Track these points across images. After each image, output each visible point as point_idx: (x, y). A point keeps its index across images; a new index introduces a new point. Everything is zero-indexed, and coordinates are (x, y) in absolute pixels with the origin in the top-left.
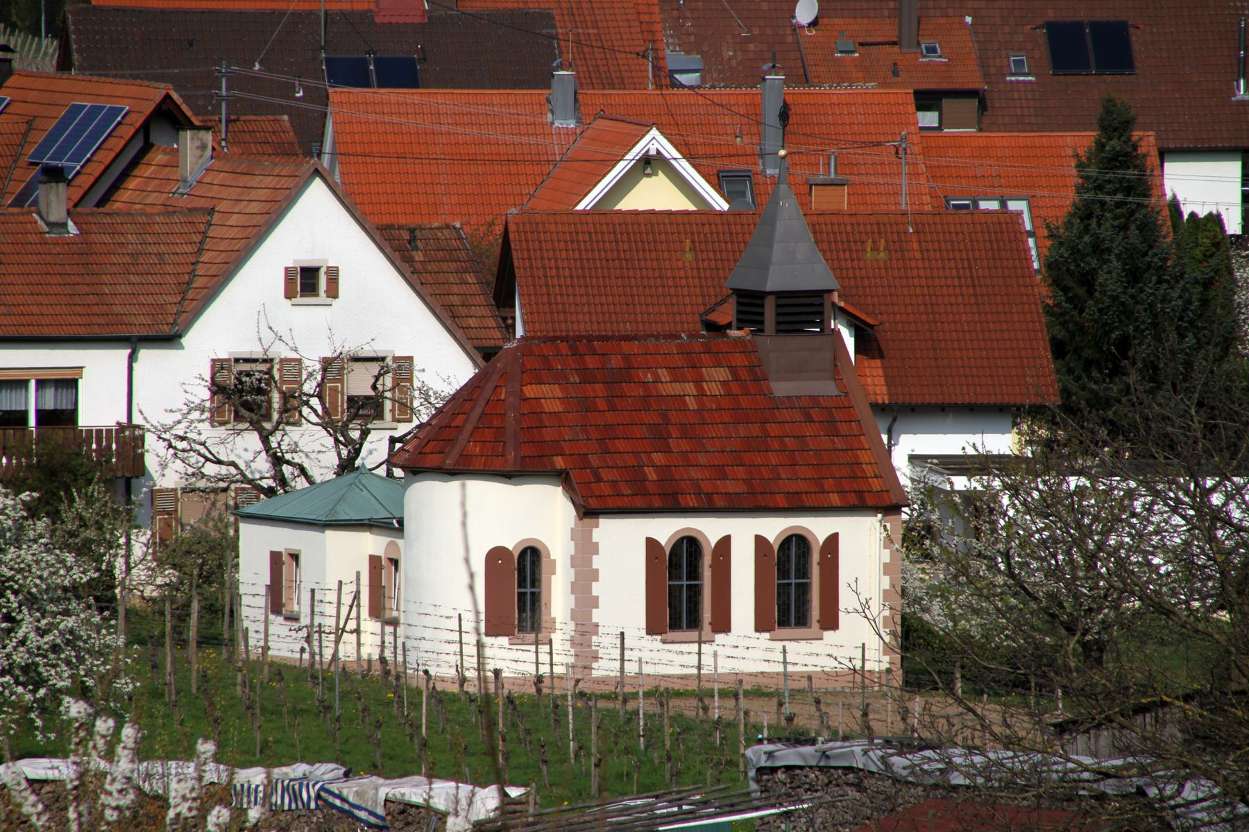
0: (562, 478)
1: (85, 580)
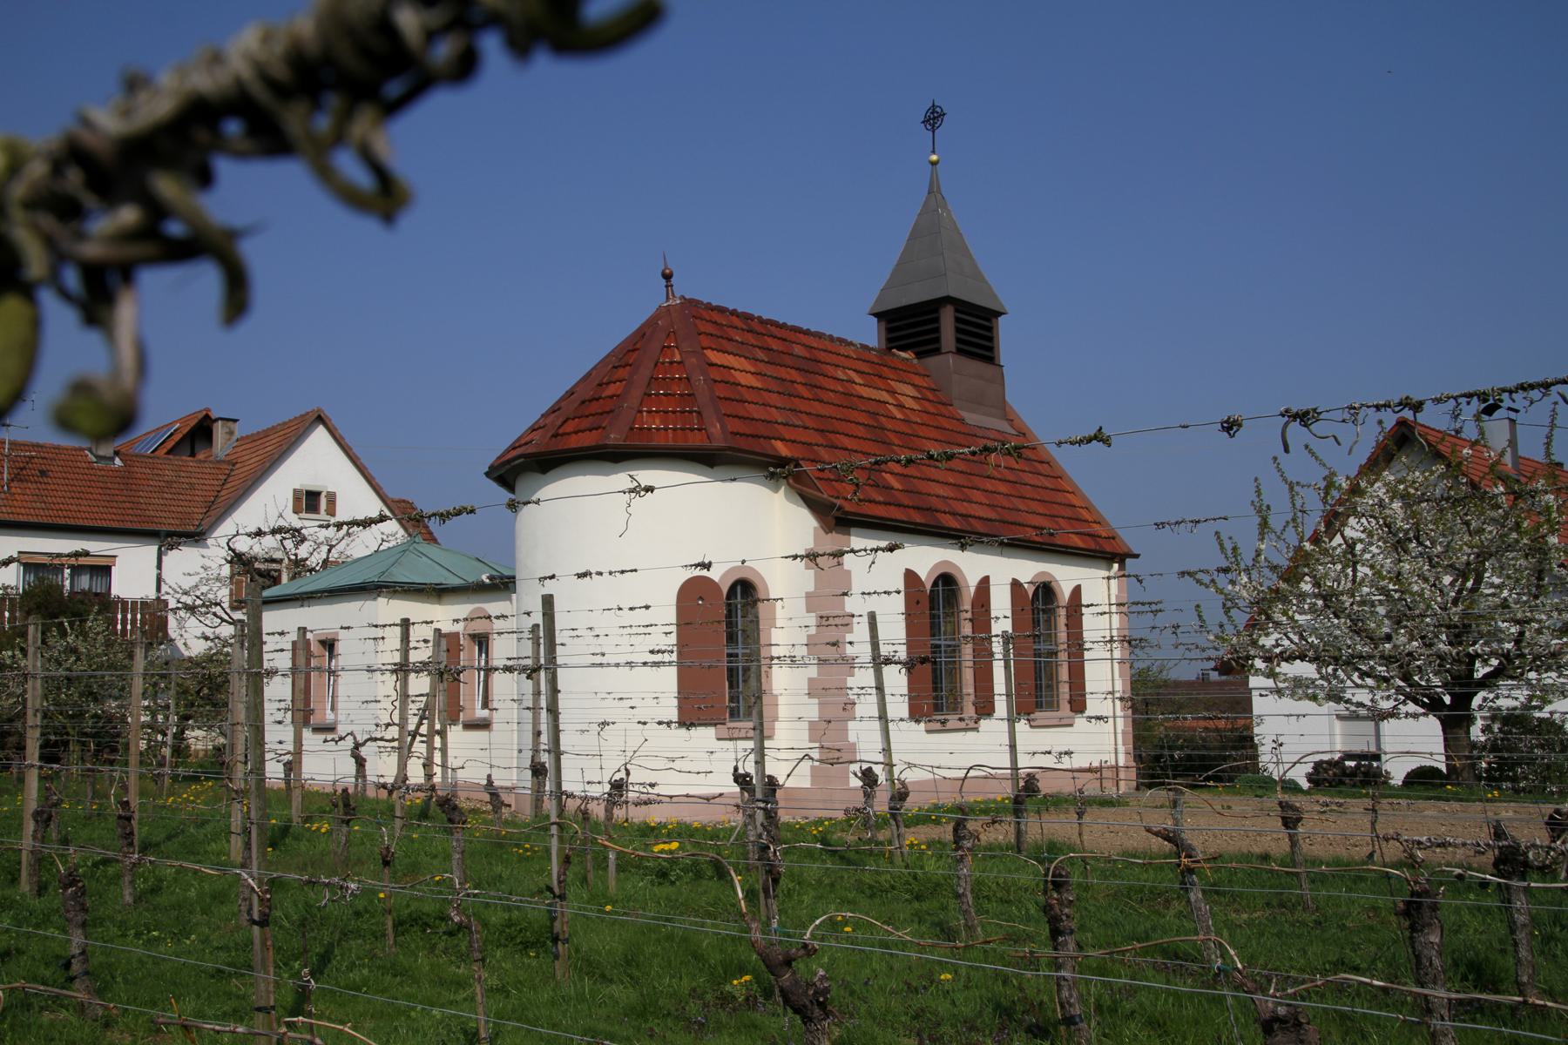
0: (773, 468)
1: (190, 1004)
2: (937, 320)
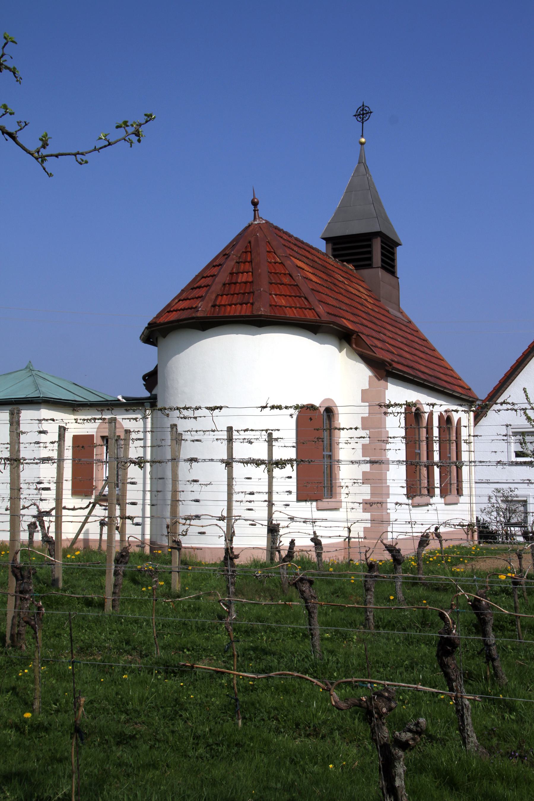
2: (370, 246)
